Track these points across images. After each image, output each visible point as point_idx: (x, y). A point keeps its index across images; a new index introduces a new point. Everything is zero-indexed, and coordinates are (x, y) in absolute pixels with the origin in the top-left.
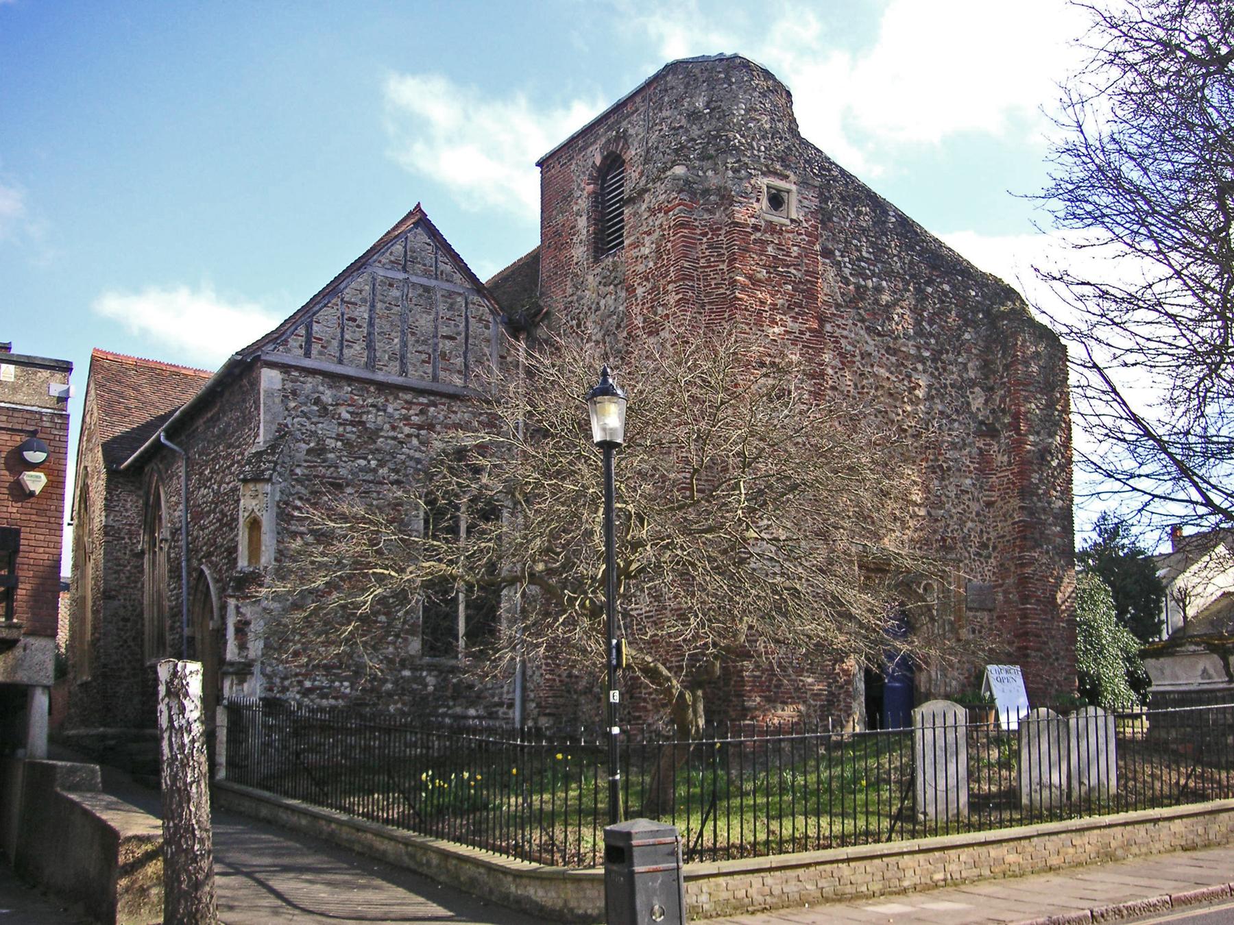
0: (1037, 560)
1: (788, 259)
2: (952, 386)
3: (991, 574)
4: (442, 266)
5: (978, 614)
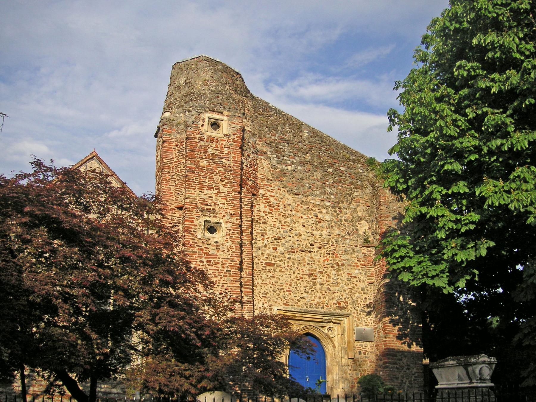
1: (221, 155)
2: (345, 220)
3: (372, 322)
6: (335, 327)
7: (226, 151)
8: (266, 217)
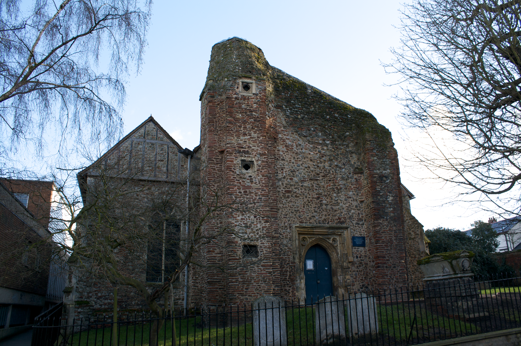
0: (381, 224)
1: (252, 109)
4: (159, 135)
6: (338, 238)
7: (255, 106)
8: (284, 155)
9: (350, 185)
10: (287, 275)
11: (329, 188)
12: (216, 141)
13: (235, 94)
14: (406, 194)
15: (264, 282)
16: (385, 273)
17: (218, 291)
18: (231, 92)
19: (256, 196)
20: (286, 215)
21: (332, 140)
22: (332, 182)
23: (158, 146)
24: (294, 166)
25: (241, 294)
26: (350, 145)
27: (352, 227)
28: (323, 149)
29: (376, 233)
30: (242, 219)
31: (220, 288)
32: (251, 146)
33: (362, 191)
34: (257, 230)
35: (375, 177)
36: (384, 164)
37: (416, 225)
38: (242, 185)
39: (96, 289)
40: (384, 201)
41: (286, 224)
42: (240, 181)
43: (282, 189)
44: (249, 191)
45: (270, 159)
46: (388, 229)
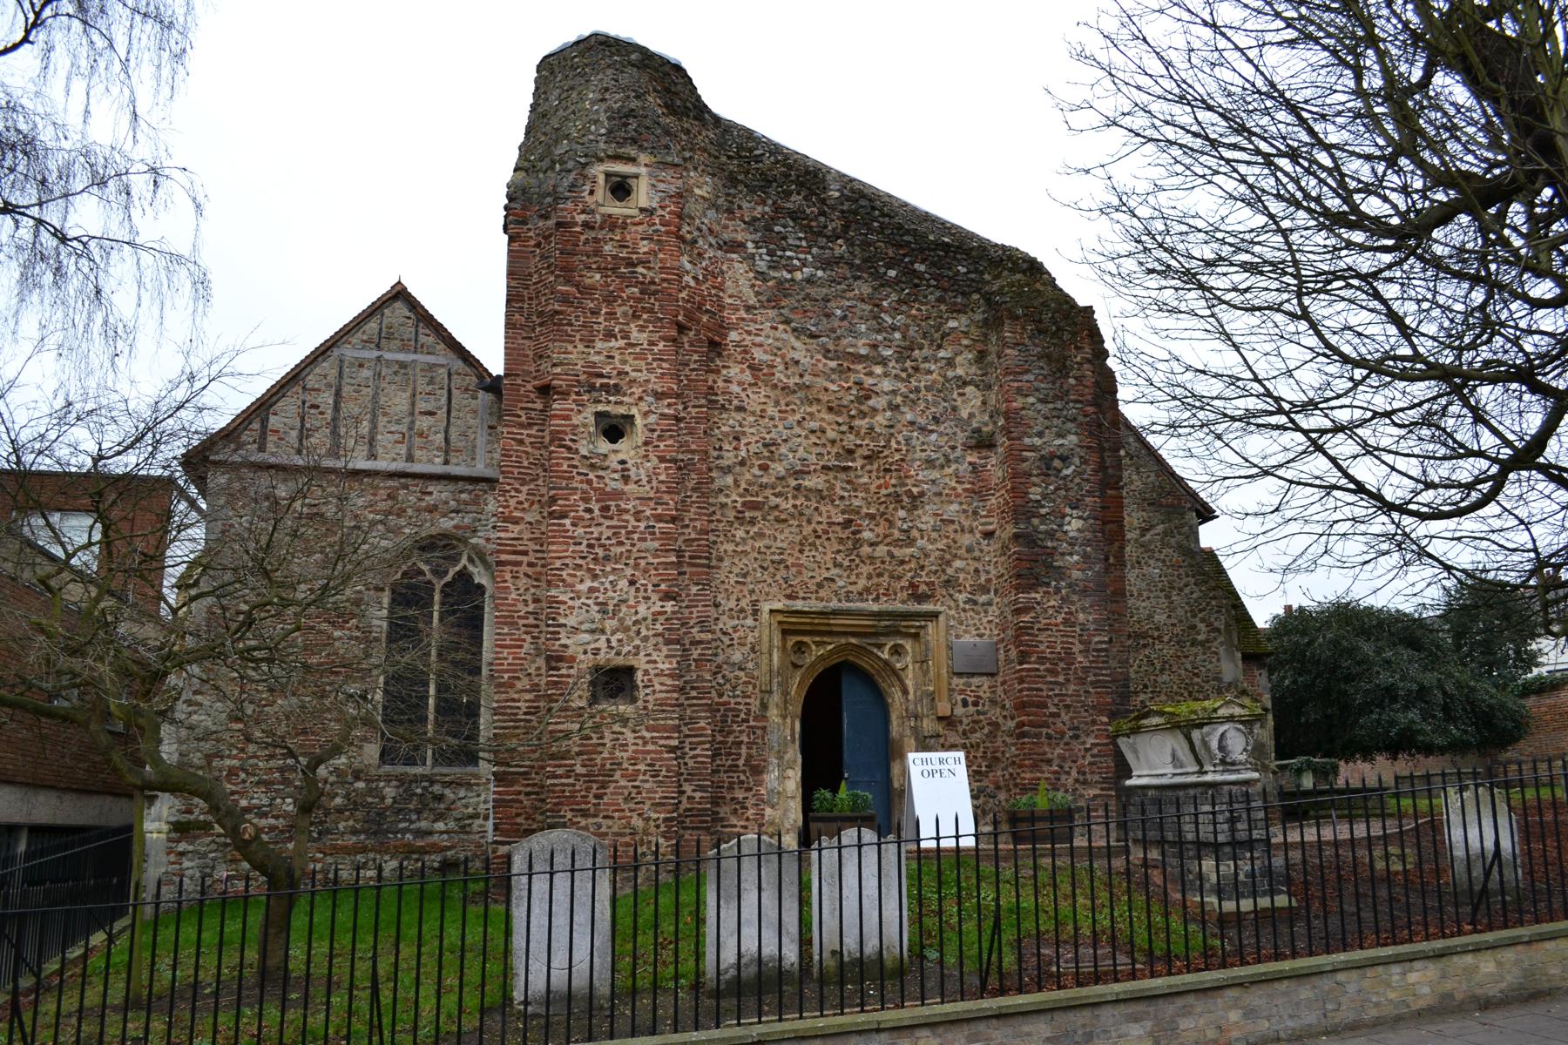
0: (1038, 603)
1: (634, 256)
5: (972, 680)
6: (908, 645)
7: (644, 247)
8: (743, 395)
9: (953, 484)
10: (740, 754)
11: (884, 492)
12: (527, 356)
13: (583, 212)
14: (1189, 505)
15: (653, 776)
16: (1045, 753)
17: (521, 802)
18: (570, 205)
19: (639, 521)
20: (745, 576)
21: (902, 344)
22: (894, 474)
23: (418, 370)
24: (775, 426)
25: (581, 810)
26: (959, 359)
27: (952, 612)
28: (870, 374)
29: (1021, 630)
30: (591, 590)
31: (528, 794)
32: (628, 369)
33: (989, 503)
34: (636, 623)
35: (1025, 460)
36: (1058, 418)
37: (1214, 603)
38: (595, 490)
39: (234, 788)
40: (1051, 535)
41: (743, 603)
42: (591, 476)
43: (734, 497)
44: (617, 506)
45: (694, 407)
46: (1059, 620)
